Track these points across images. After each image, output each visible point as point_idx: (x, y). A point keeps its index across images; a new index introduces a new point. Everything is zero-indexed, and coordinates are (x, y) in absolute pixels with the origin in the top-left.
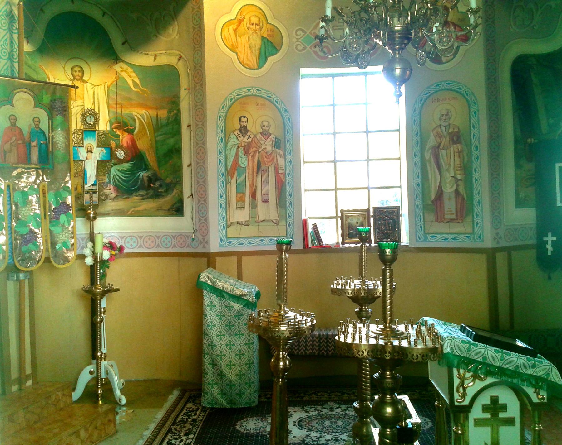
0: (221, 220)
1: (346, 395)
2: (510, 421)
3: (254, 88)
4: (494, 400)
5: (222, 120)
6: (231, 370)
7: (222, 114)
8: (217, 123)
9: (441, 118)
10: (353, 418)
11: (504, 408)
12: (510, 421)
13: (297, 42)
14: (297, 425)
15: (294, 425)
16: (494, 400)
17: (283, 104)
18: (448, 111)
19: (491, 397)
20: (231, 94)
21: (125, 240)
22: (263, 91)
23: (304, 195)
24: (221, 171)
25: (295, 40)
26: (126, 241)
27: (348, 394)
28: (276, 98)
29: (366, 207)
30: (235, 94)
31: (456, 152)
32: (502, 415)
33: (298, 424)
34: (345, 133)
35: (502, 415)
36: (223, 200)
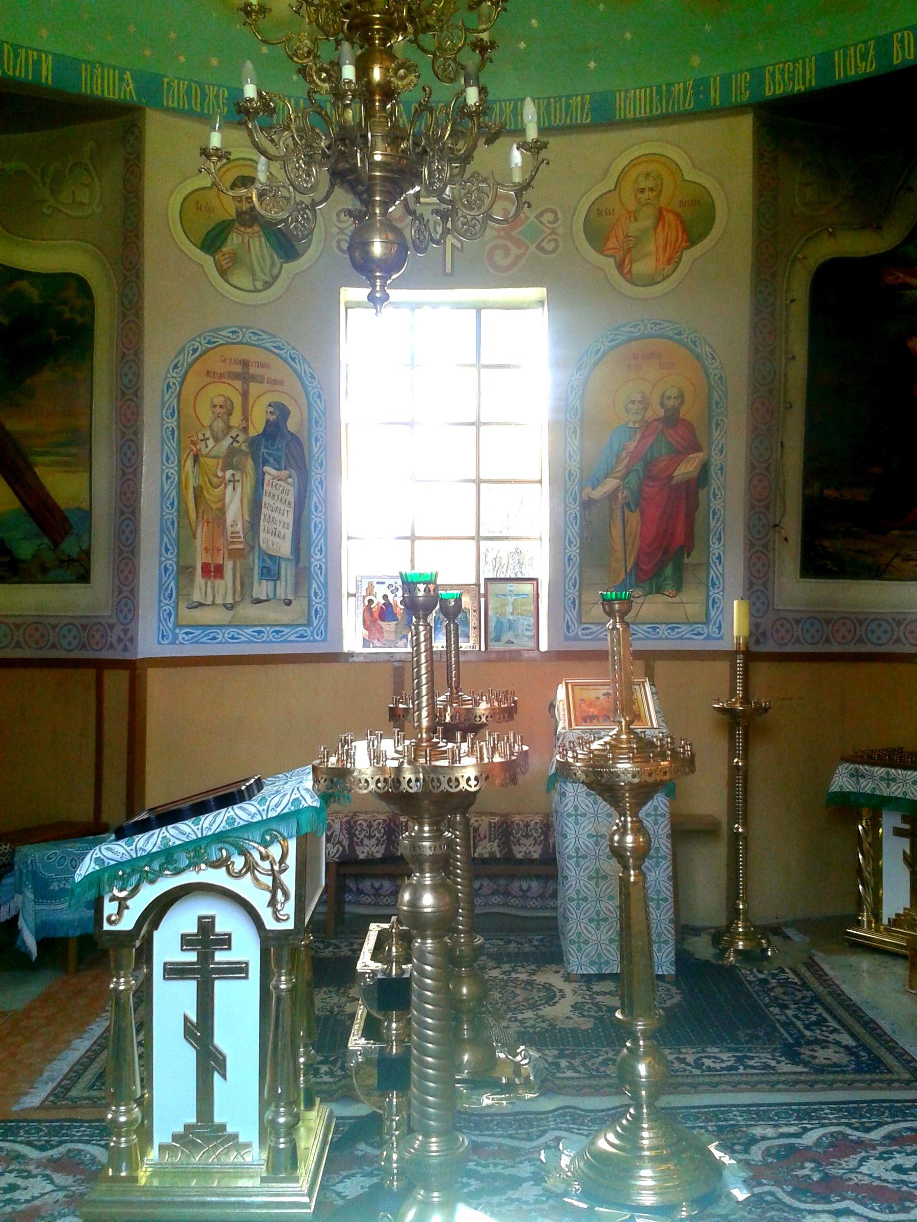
0: (569, 588)
1: (513, 945)
2: (238, 970)
3: (244, 330)
4: (206, 925)
5: (172, 393)
6: (598, 887)
7: (172, 380)
8: (163, 397)
9: (630, 406)
10: (522, 986)
11: (226, 942)
12: (238, 970)
13: (338, 234)
14: (557, 992)
15: (561, 991)
16: (206, 925)
17: (308, 363)
18: (228, 399)
19: (200, 918)
20: (194, 340)
21: (892, 634)
22: (265, 336)
23: (345, 543)
24: (171, 485)
25: (335, 230)
26: (889, 635)
27: (518, 943)
28: (292, 352)
29: (474, 582)
30: (202, 341)
31: (238, 481)
32: (220, 956)
33: (554, 991)
34: (510, 424)
35: (220, 956)
36: (574, 549)
